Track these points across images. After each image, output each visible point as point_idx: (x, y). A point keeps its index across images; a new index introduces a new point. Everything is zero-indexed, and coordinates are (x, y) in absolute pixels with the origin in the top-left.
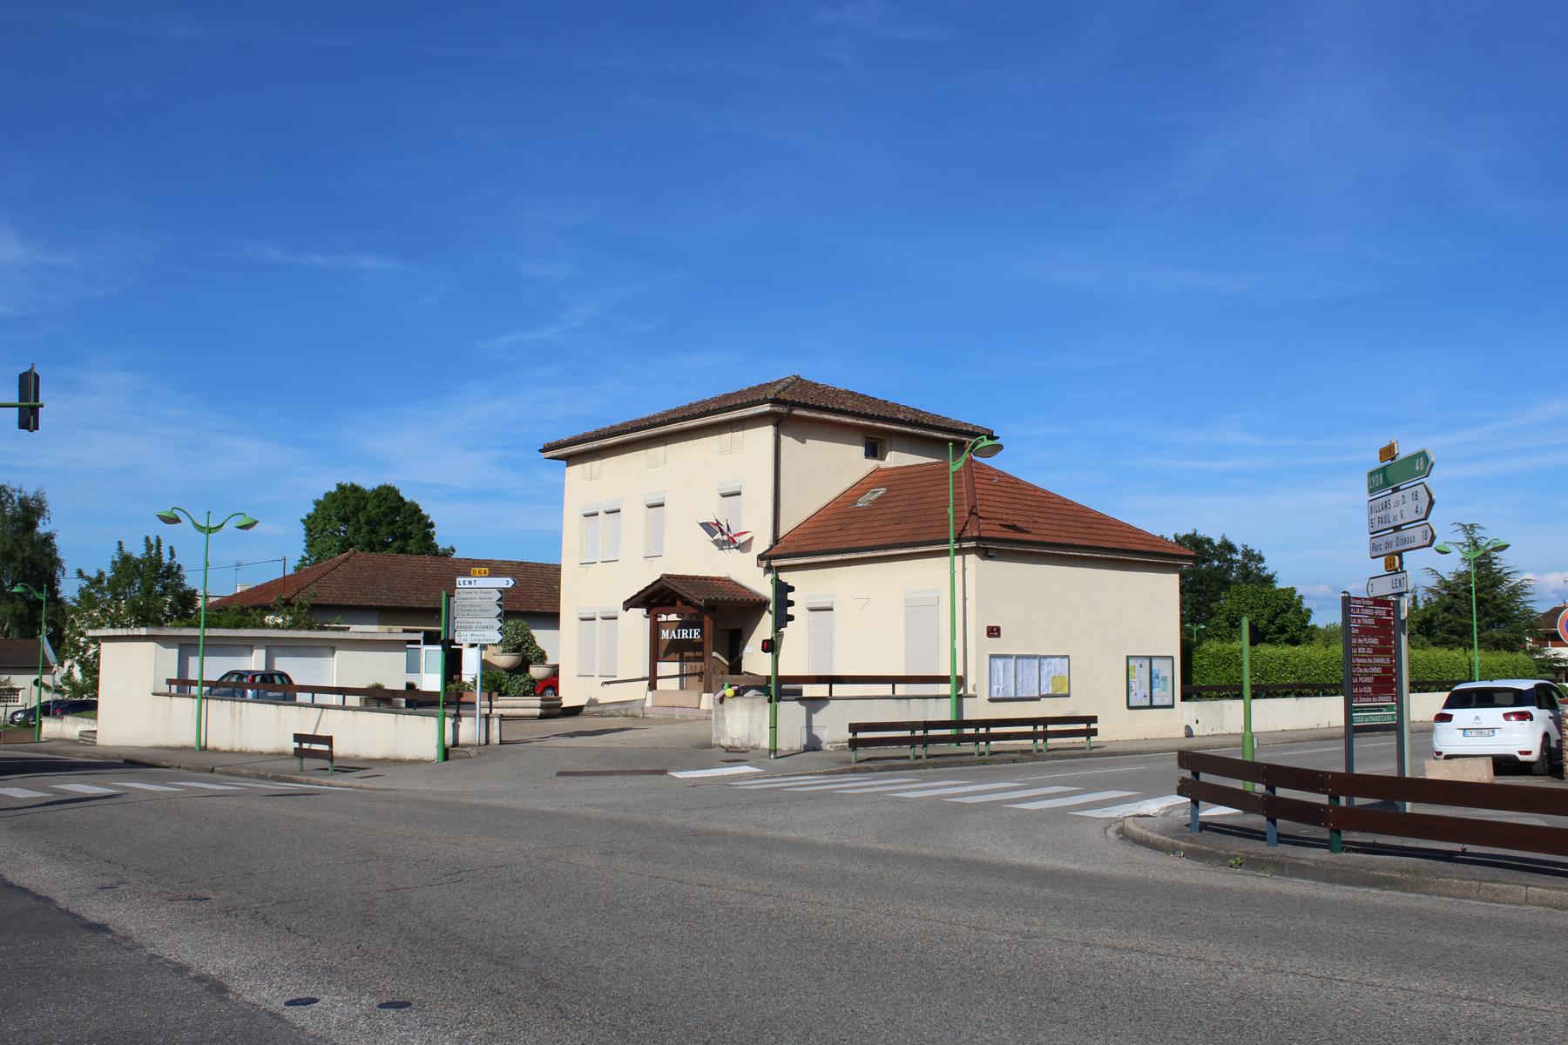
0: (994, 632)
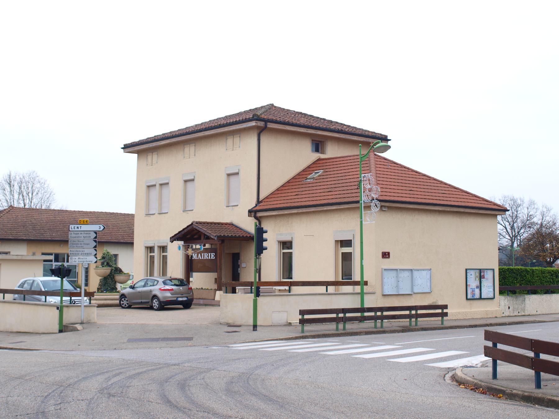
0: (386, 255)
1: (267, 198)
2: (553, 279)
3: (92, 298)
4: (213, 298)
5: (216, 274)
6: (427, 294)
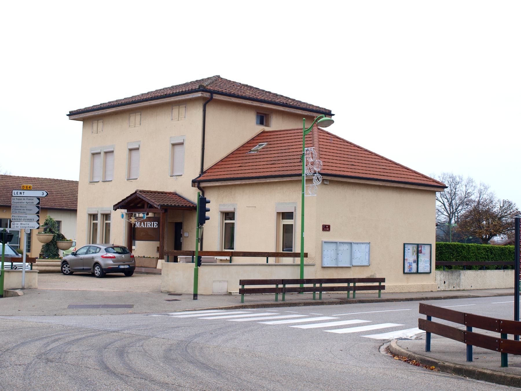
0: (326, 228)
1: (211, 168)
2: (487, 255)
3: (33, 264)
4: (154, 266)
6: (365, 267)
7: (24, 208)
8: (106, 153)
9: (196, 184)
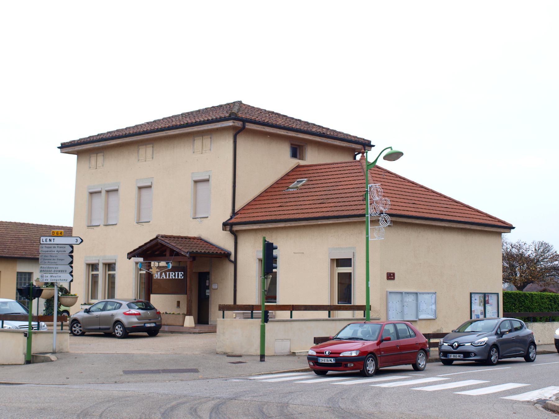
0: (391, 276)
1: (243, 209)
2: (551, 305)
3: (64, 323)
4: (181, 324)
5: (186, 296)
6: (432, 321)
7: (54, 258)
8: (108, 192)
9: (228, 228)
